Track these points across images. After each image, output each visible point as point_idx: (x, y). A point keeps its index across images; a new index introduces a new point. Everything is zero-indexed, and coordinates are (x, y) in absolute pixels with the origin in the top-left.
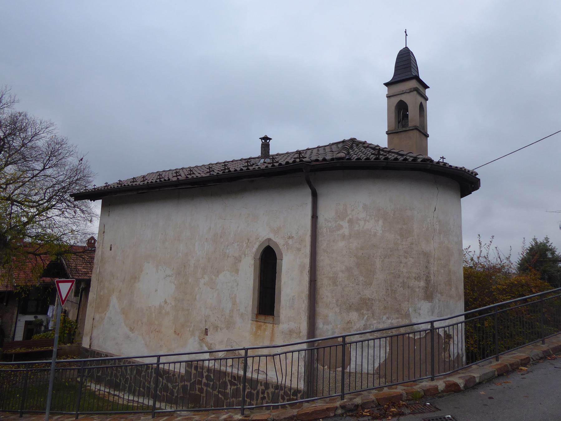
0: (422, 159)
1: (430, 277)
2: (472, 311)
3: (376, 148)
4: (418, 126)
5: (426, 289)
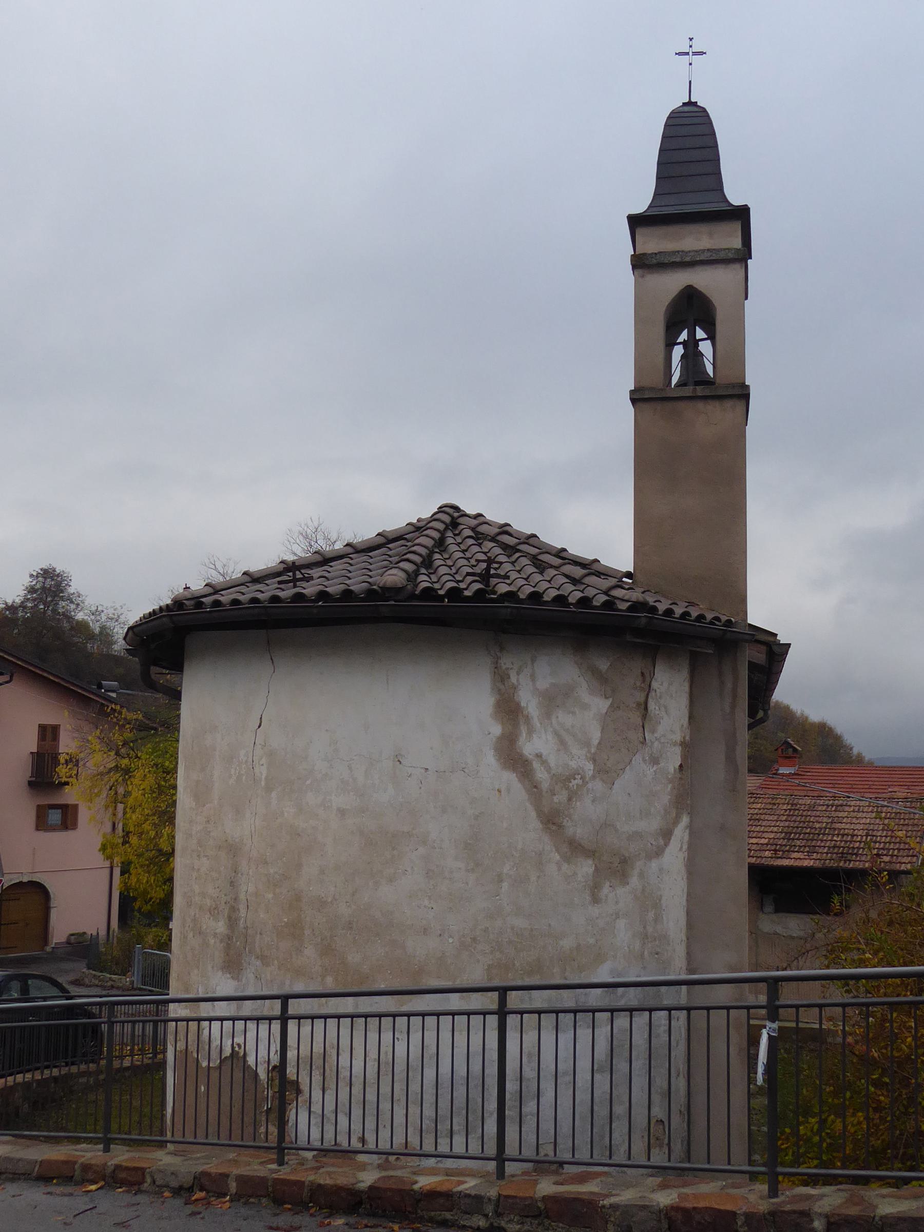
0: (630, 603)
1: (238, 909)
2: (14, 1024)
5: (228, 941)
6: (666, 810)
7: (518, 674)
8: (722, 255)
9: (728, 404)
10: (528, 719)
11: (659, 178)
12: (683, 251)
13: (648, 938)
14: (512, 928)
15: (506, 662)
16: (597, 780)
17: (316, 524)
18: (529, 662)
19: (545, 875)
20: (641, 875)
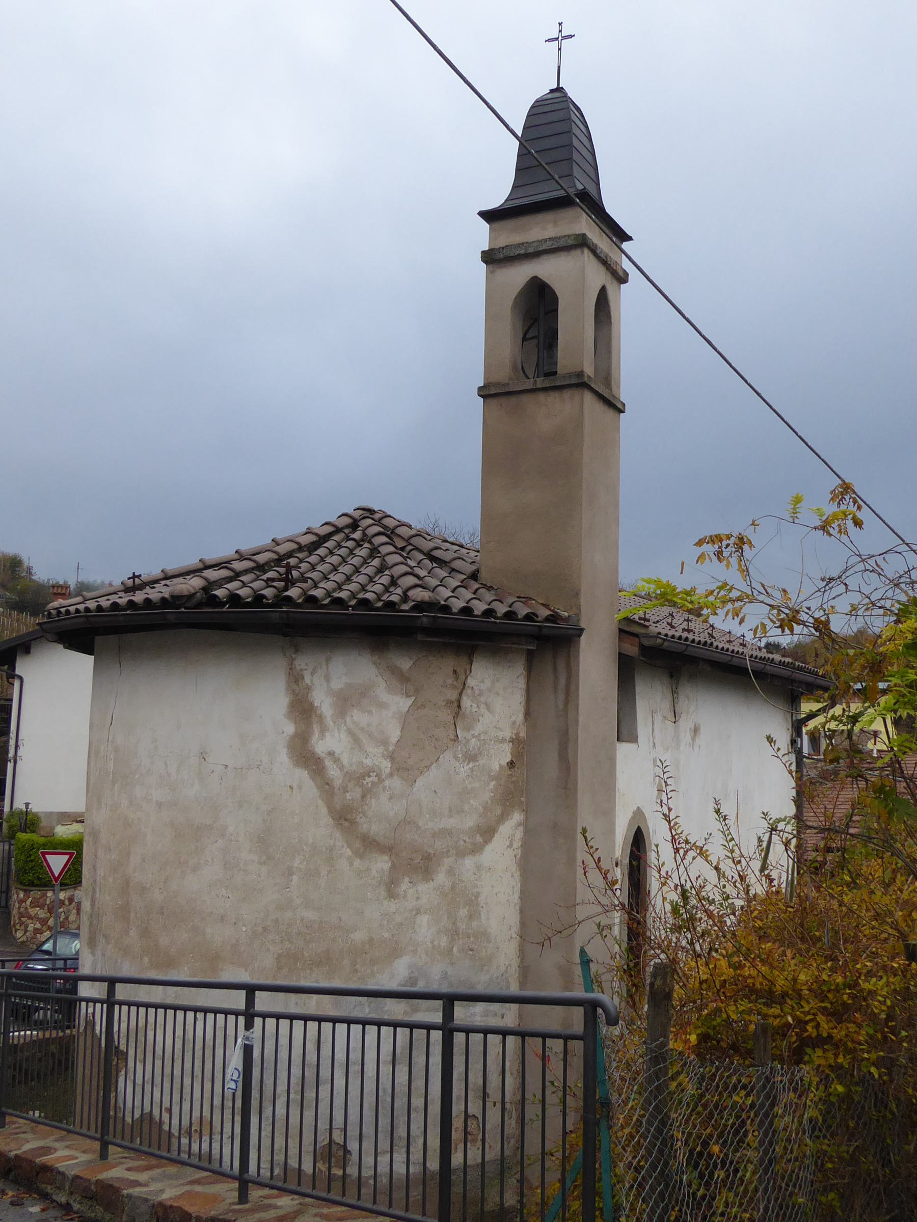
3: (520, 134)
4: (589, 377)
6: (485, 808)
7: (312, 674)
8: (562, 243)
9: (567, 394)
10: (321, 718)
11: (518, 170)
12: (527, 243)
13: (458, 935)
14: (302, 920)
15: (303, 662)
16: (396, 777)
17: (433, 521)
18: (324, 663)
19: (335, 870)
20: (451, 872)
